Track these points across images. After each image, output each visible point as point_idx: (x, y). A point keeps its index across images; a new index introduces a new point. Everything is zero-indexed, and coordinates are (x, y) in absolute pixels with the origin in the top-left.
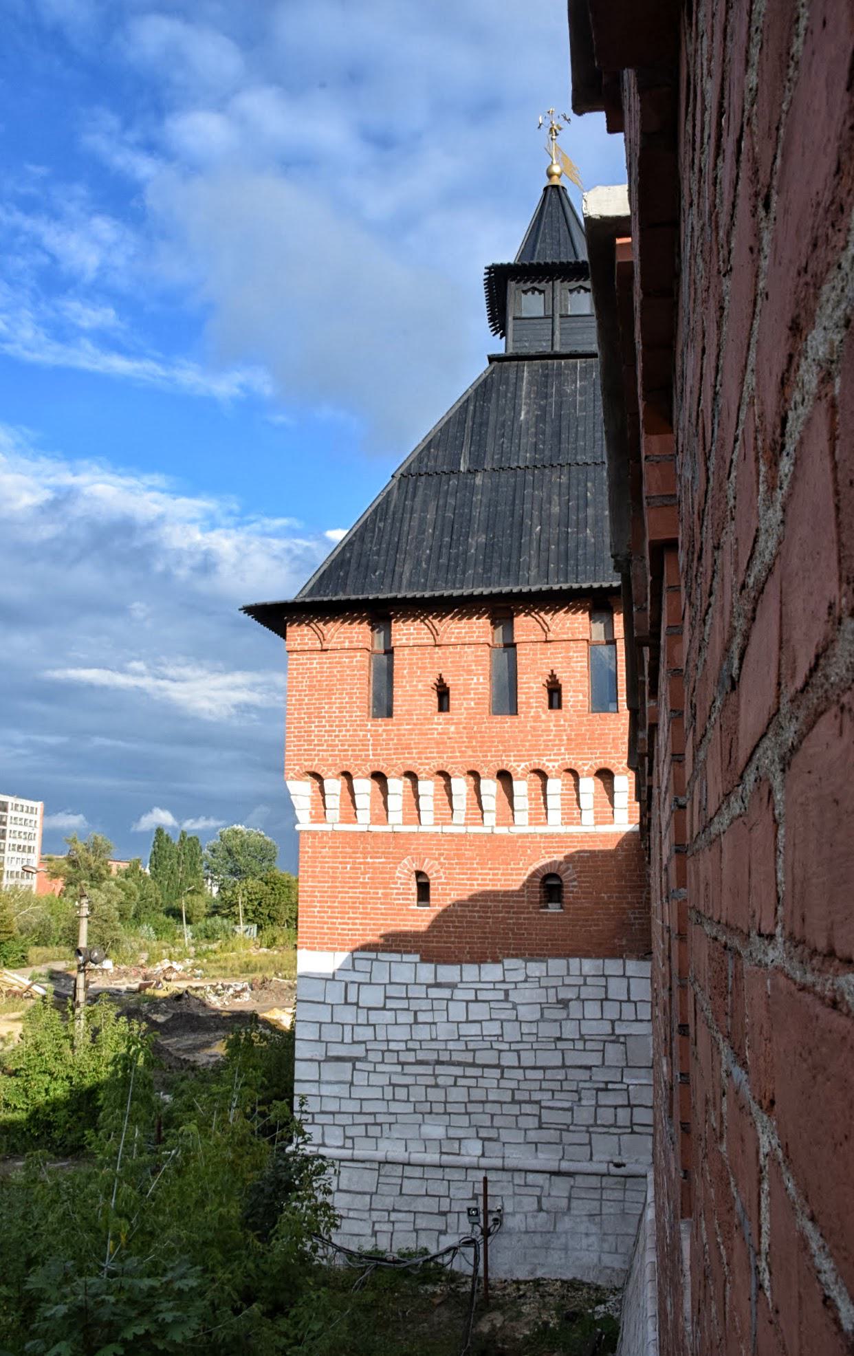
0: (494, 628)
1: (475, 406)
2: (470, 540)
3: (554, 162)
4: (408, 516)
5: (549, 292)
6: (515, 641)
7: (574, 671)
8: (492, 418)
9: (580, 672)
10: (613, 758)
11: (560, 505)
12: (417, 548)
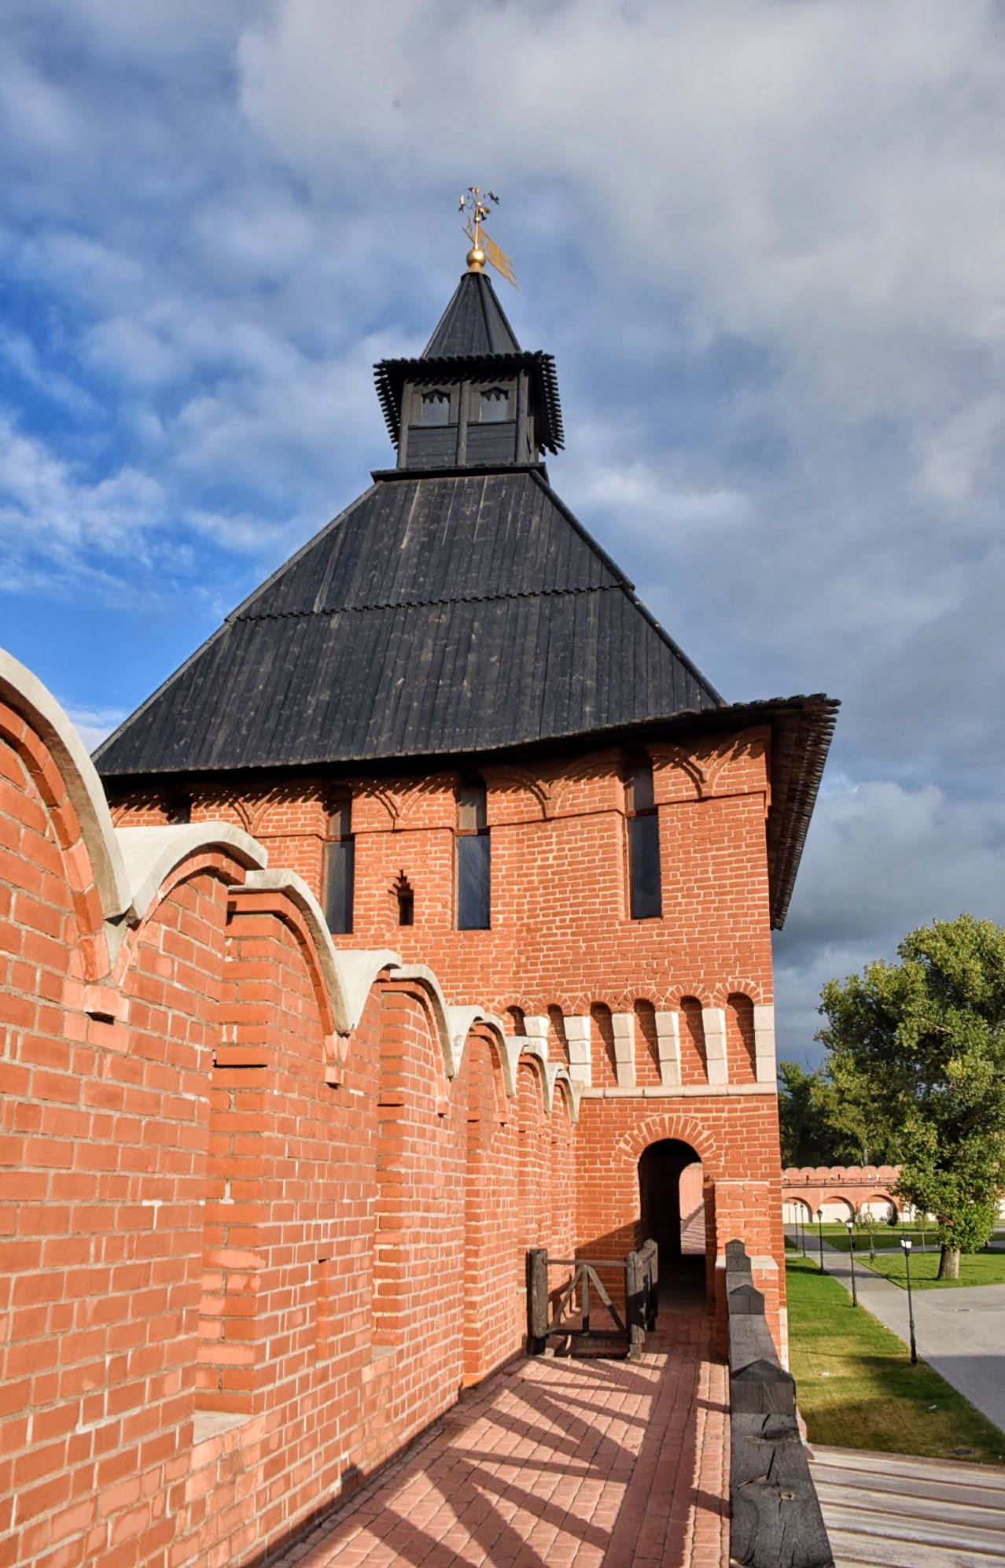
0: (330, 815)
1: (346, 535)
2: (309, 698)
3: (477, 247)
4: (236, 669)
5: (455, 398)
6: (353, 830)
7: (431, 872)
8: (365, 546)
9: (439, 873)
10: (481, 994)
11: (433, 652)
12: (240, 710)
